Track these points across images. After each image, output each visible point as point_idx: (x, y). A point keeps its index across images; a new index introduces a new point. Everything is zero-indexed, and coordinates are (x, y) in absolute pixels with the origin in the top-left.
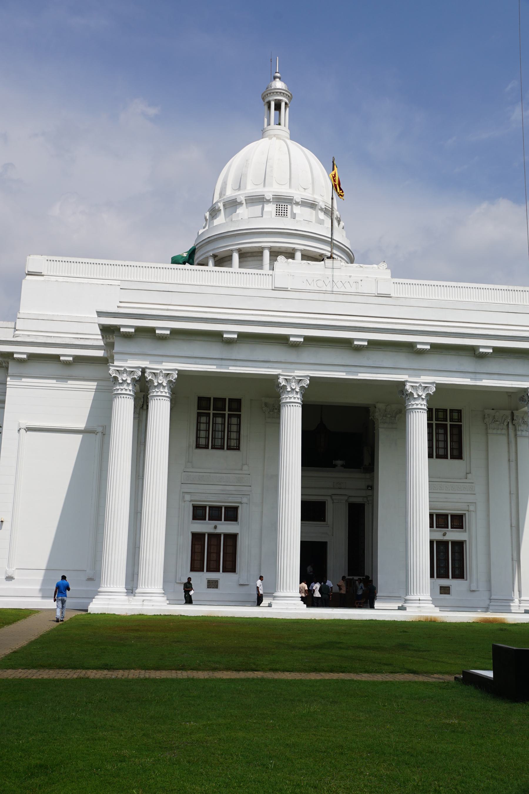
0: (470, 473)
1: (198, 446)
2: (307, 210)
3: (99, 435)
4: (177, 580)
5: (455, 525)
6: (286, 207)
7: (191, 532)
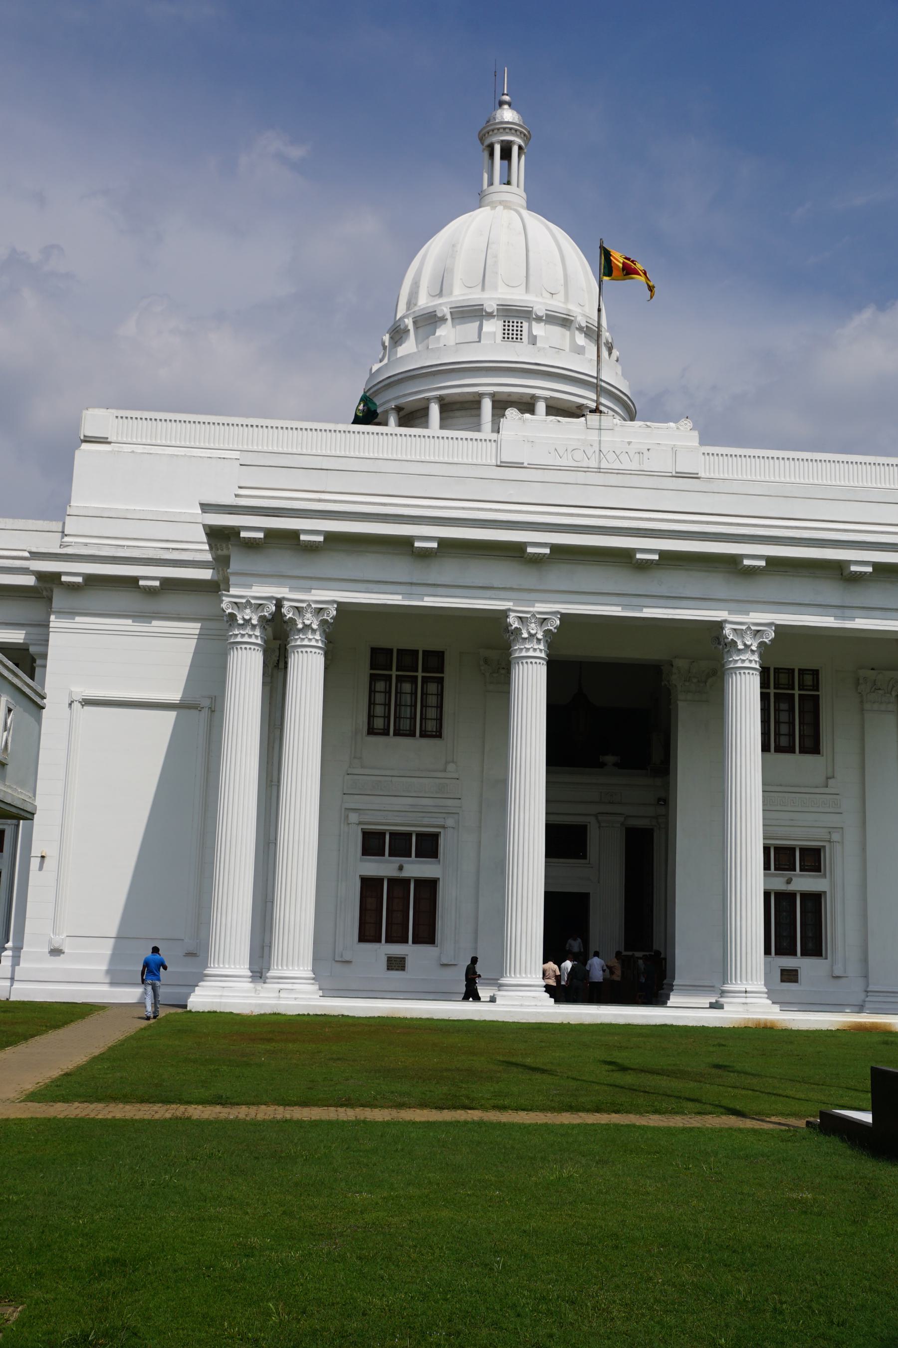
2: (556, 330)
7: (360, 876)
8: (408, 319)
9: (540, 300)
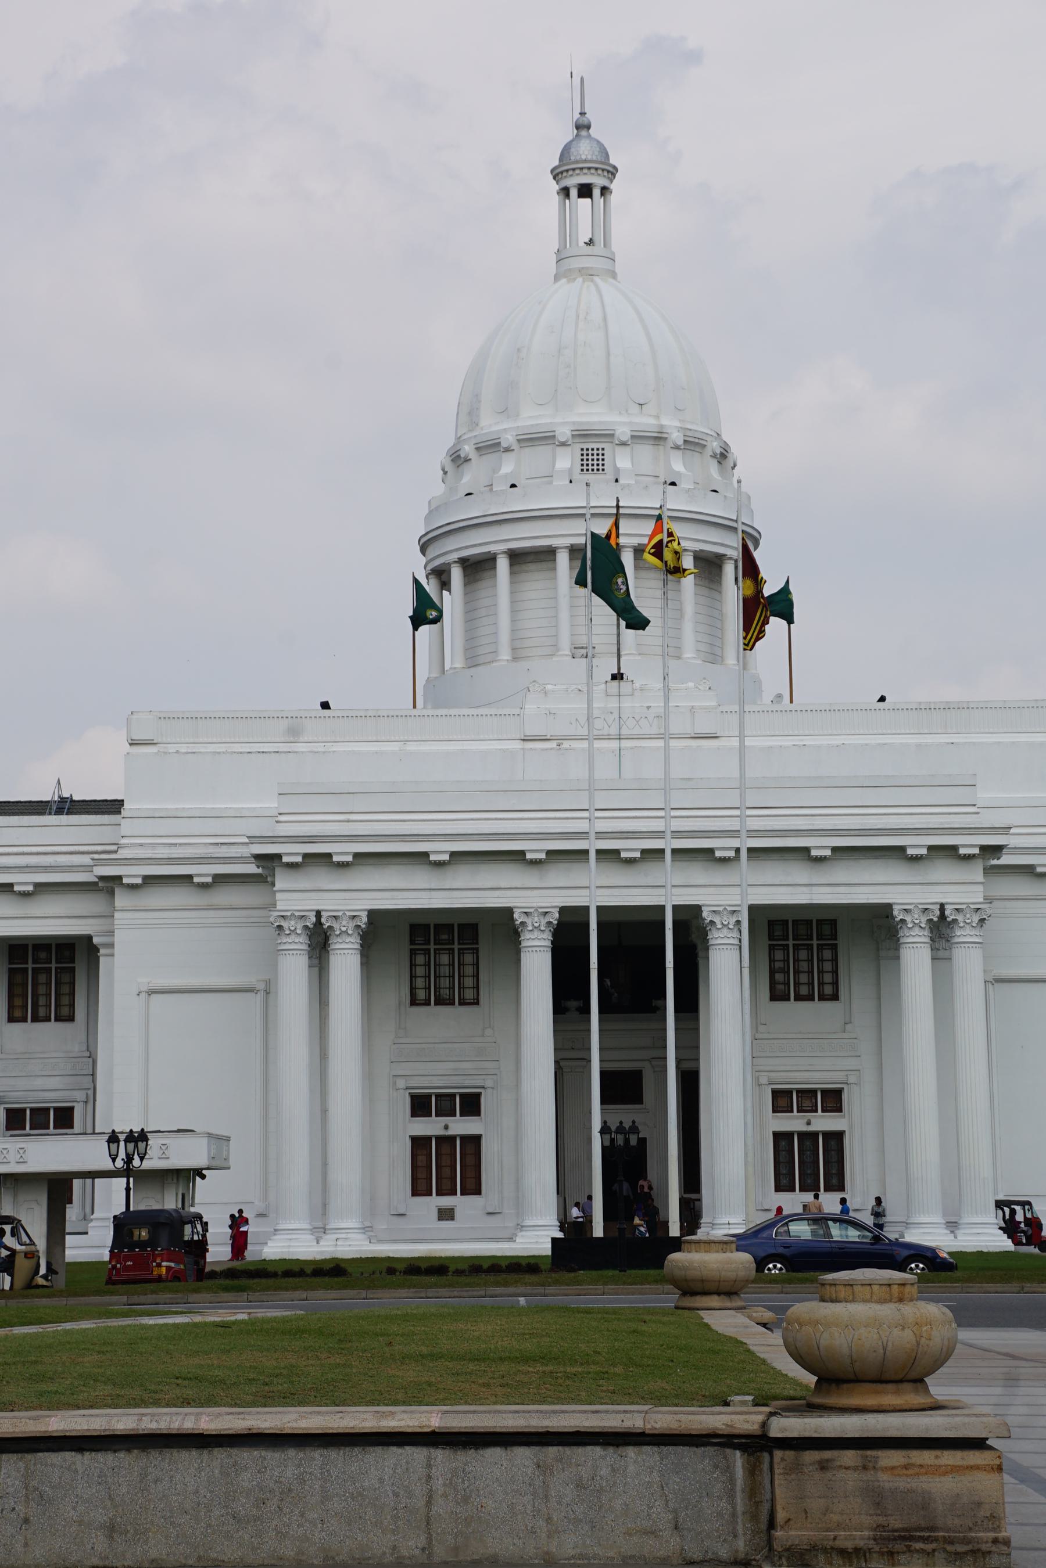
0: (851, 1022)
1: (414, 1002)
2: (645, 451)
3: (261, 994)
6: (600, 452)
9: (624, 419)
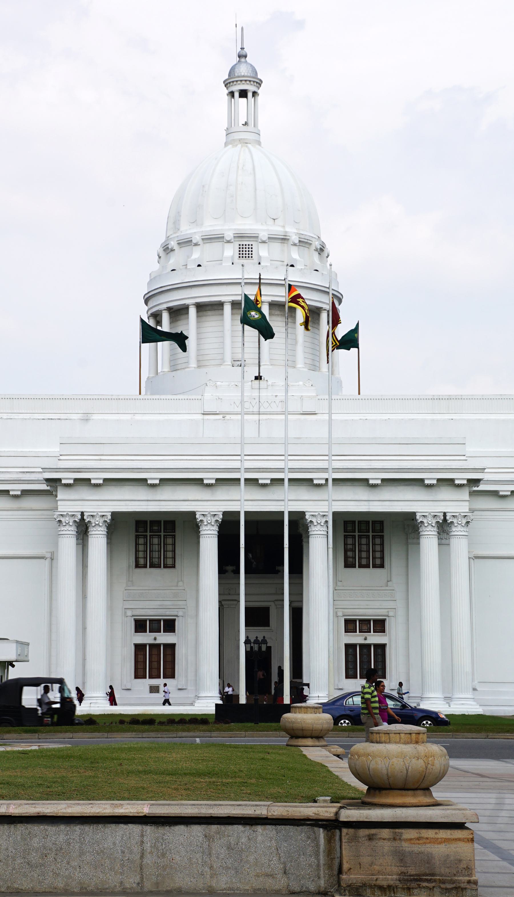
1: (137, 566)
3: (49, 560)
4: (123, 686)
5: (378, 629)
7: (134, 644)
8: (173, 241)
9: (264, 227)
